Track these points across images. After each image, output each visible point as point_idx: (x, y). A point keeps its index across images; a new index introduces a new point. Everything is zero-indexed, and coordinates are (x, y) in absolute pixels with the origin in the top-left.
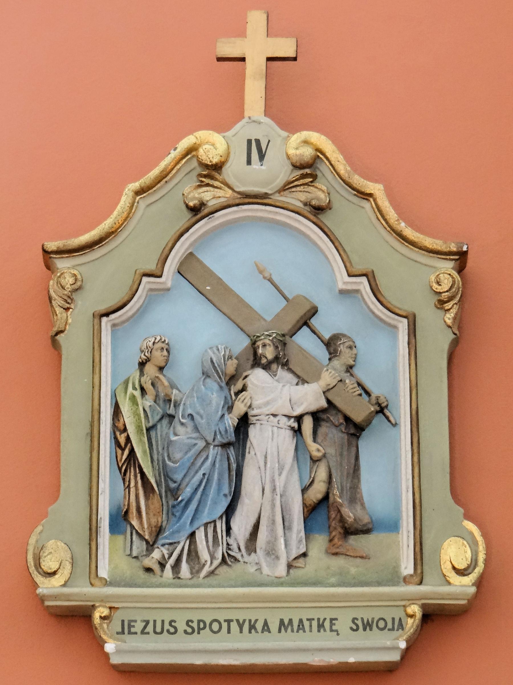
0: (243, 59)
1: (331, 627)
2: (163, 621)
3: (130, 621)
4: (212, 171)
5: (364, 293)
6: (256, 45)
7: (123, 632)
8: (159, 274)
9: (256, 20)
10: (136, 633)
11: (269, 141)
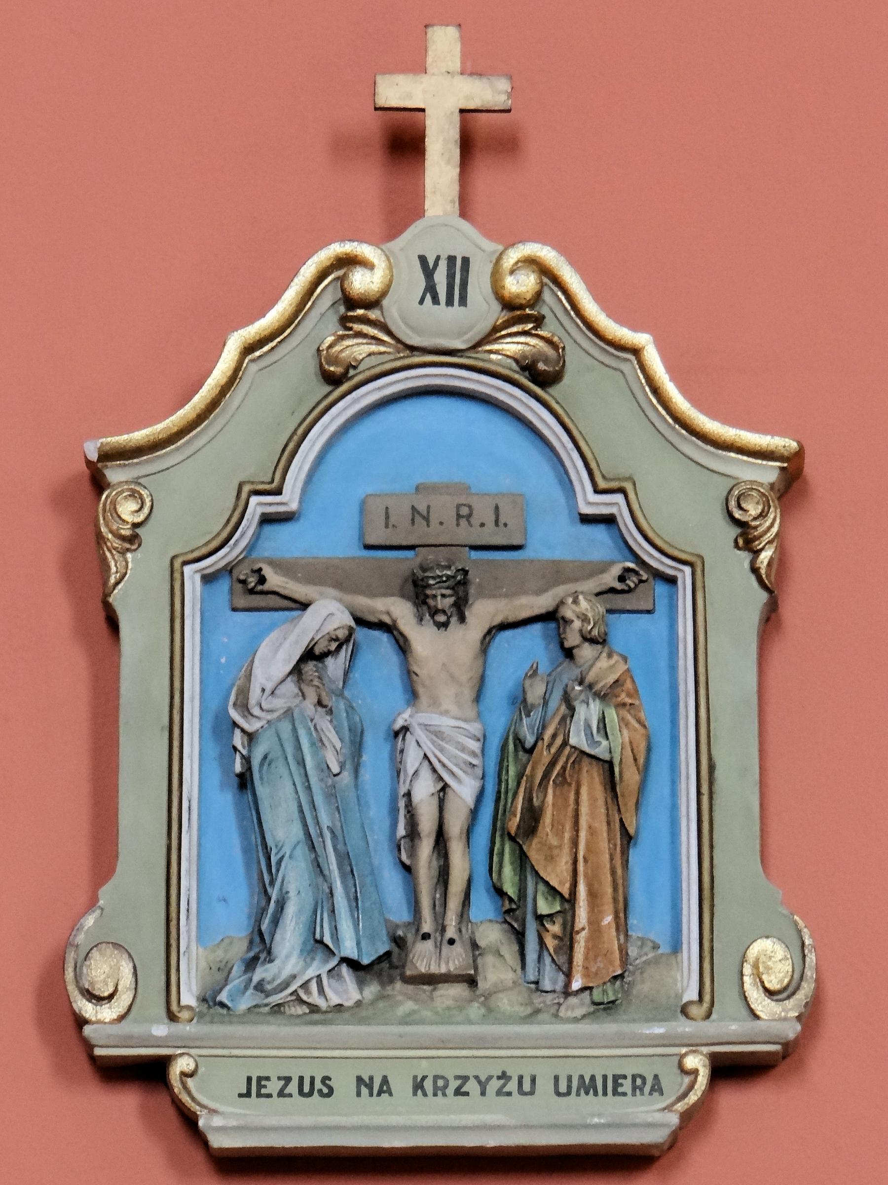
0: (423, 110)
2: (312, 1079)
3: (260, 1079)
4: (354, 309)
9: (444, 43)
10: (269, 1096)
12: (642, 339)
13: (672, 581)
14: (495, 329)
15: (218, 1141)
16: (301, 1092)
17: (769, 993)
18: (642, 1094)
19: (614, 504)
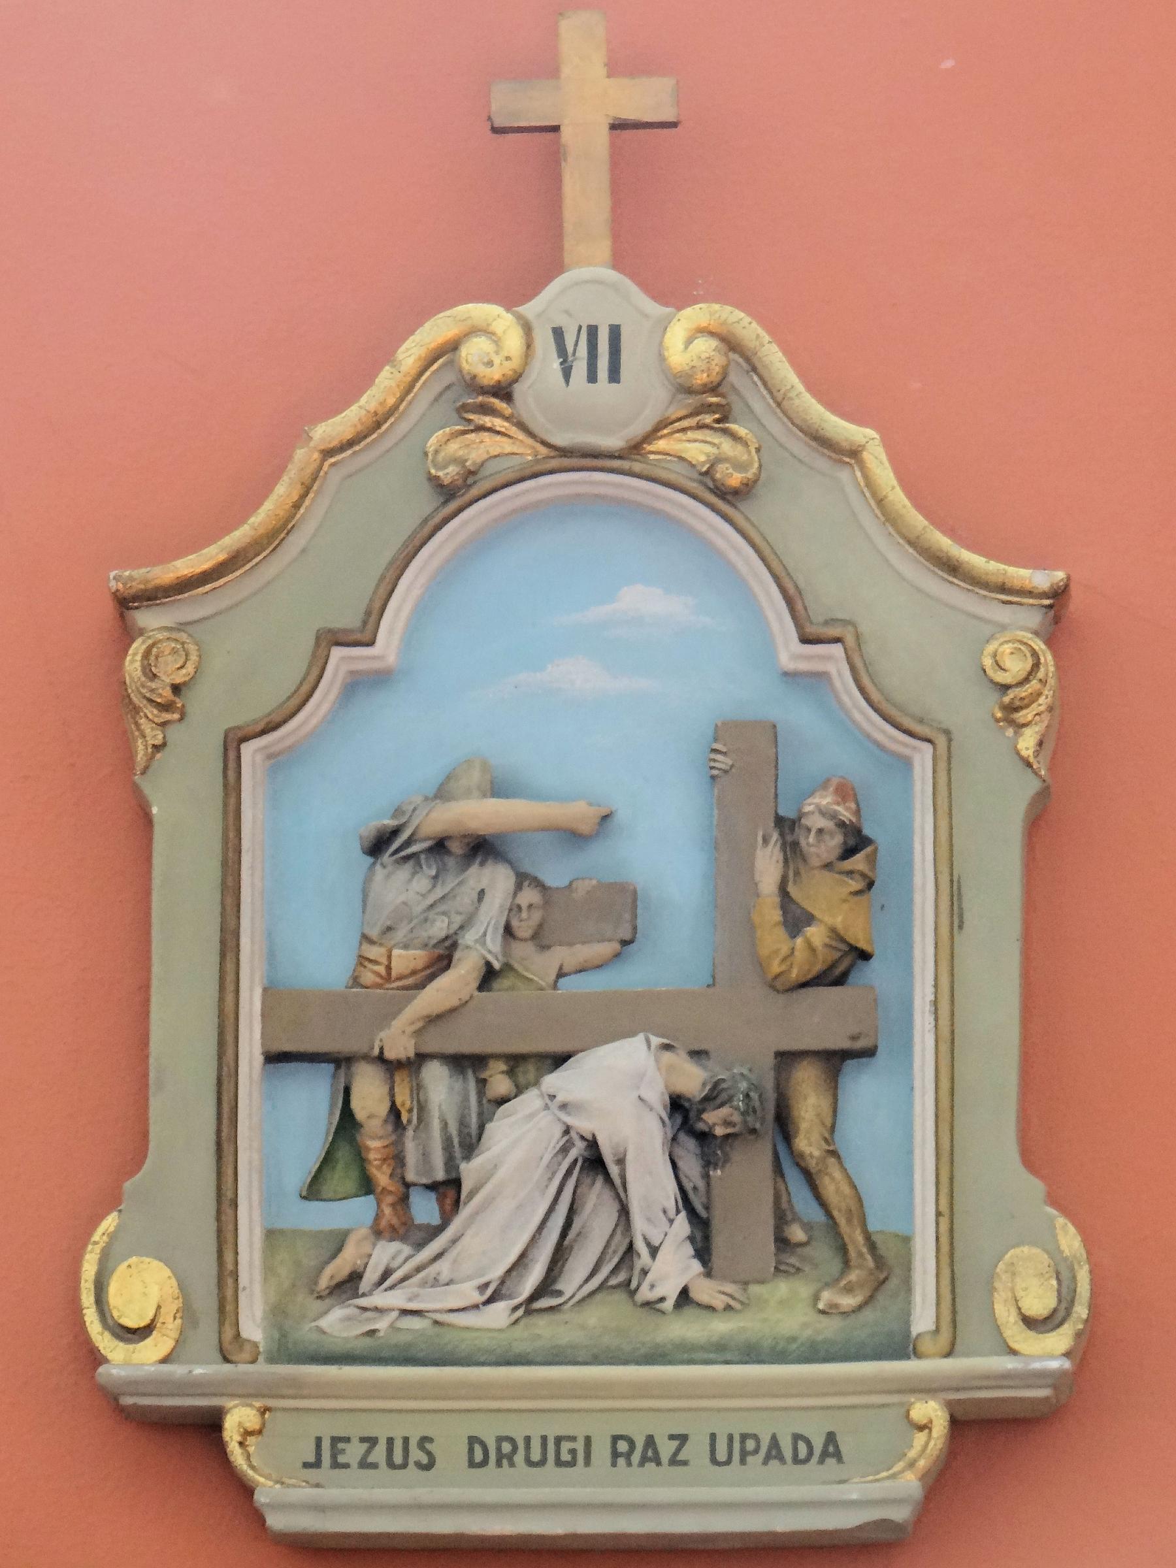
0: (556, 129)
1: (334, 1457)
2: (406, 1440)
3: (335, 1440)
5: (838, 684)
6: (588, 95)
7: (317, 1464)
8: (366, 637)
9: (582, 43)
10: (346, 1466)
13: (906, 763)
15: (276, 1522)
16: (472, 1464)
17: (1030, 1323)
18: (512, 1464)
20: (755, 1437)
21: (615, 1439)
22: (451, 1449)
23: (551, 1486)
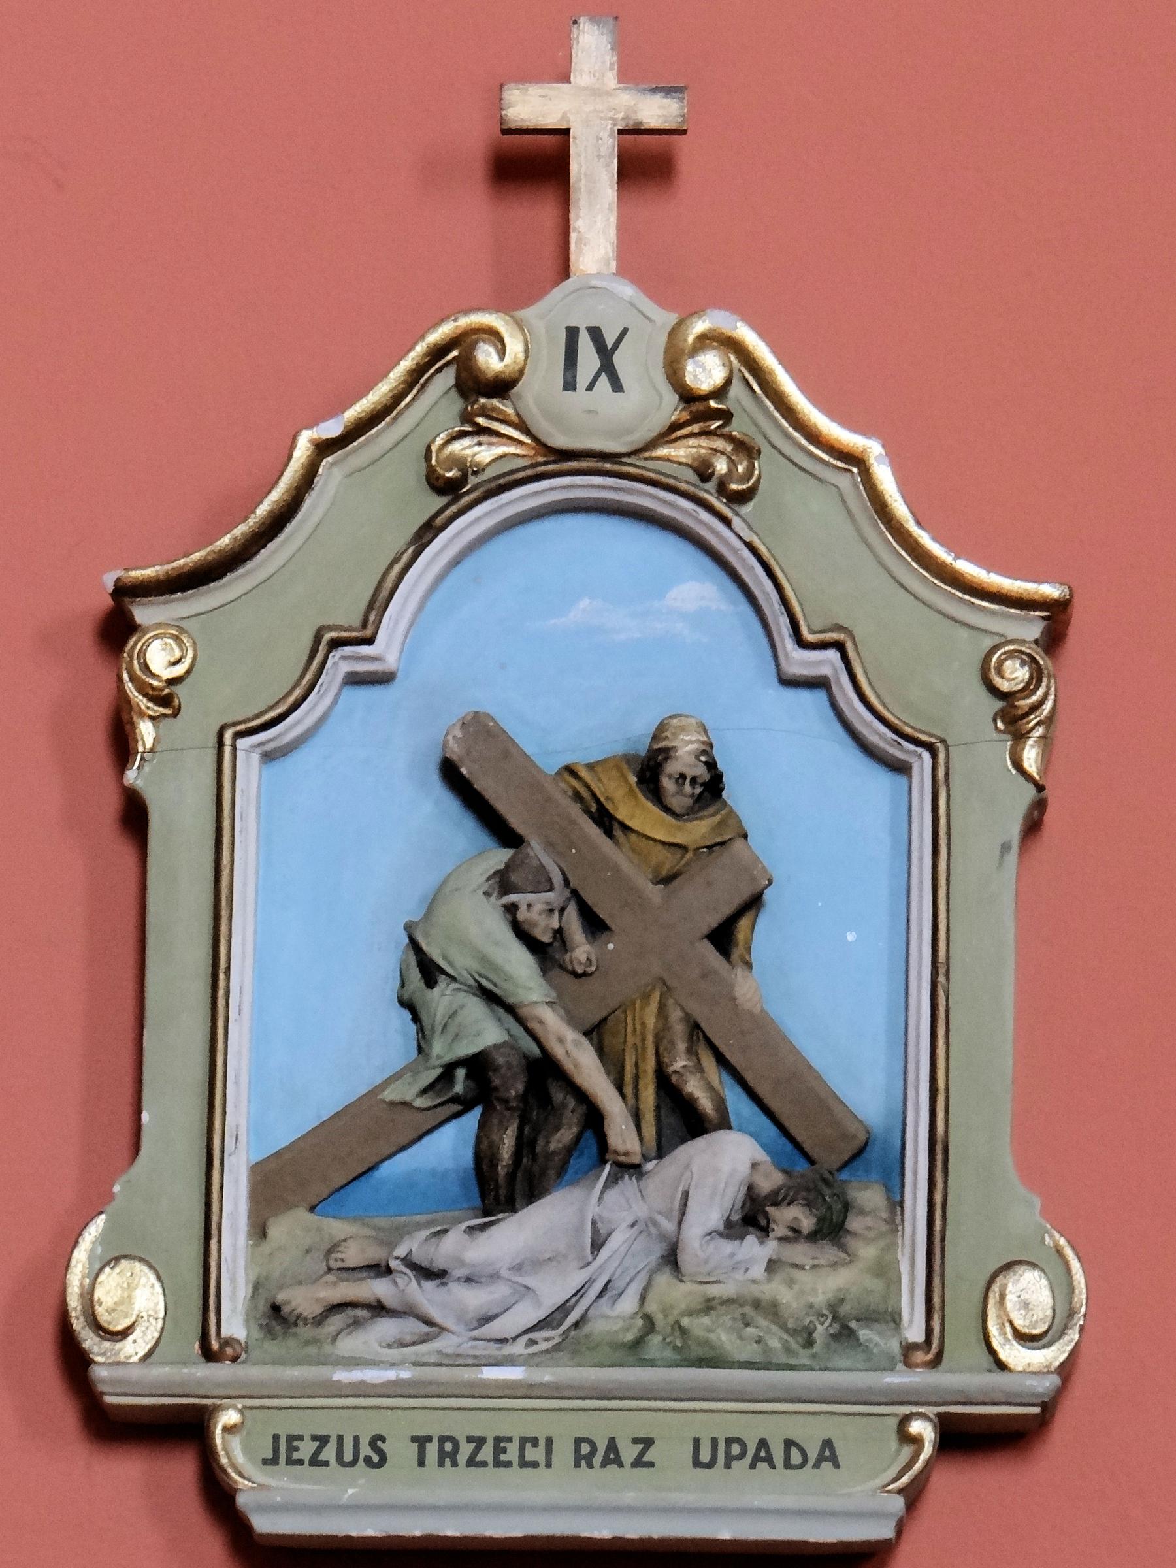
2: (356, 1440)
3: (291, 1438)
4: (482, 391)
8: (368, 633)
9: (592, 46)
10: (300, 1462)
11: (625, 331)
12: (873, 448)
14: (675, 427)
16: (697, 1463)
18: (590, 1465)
19: (800, 661)
20: (738, 1440)
21: (578, 1441)
22: (671, 1453)
23: (487, 1487)
